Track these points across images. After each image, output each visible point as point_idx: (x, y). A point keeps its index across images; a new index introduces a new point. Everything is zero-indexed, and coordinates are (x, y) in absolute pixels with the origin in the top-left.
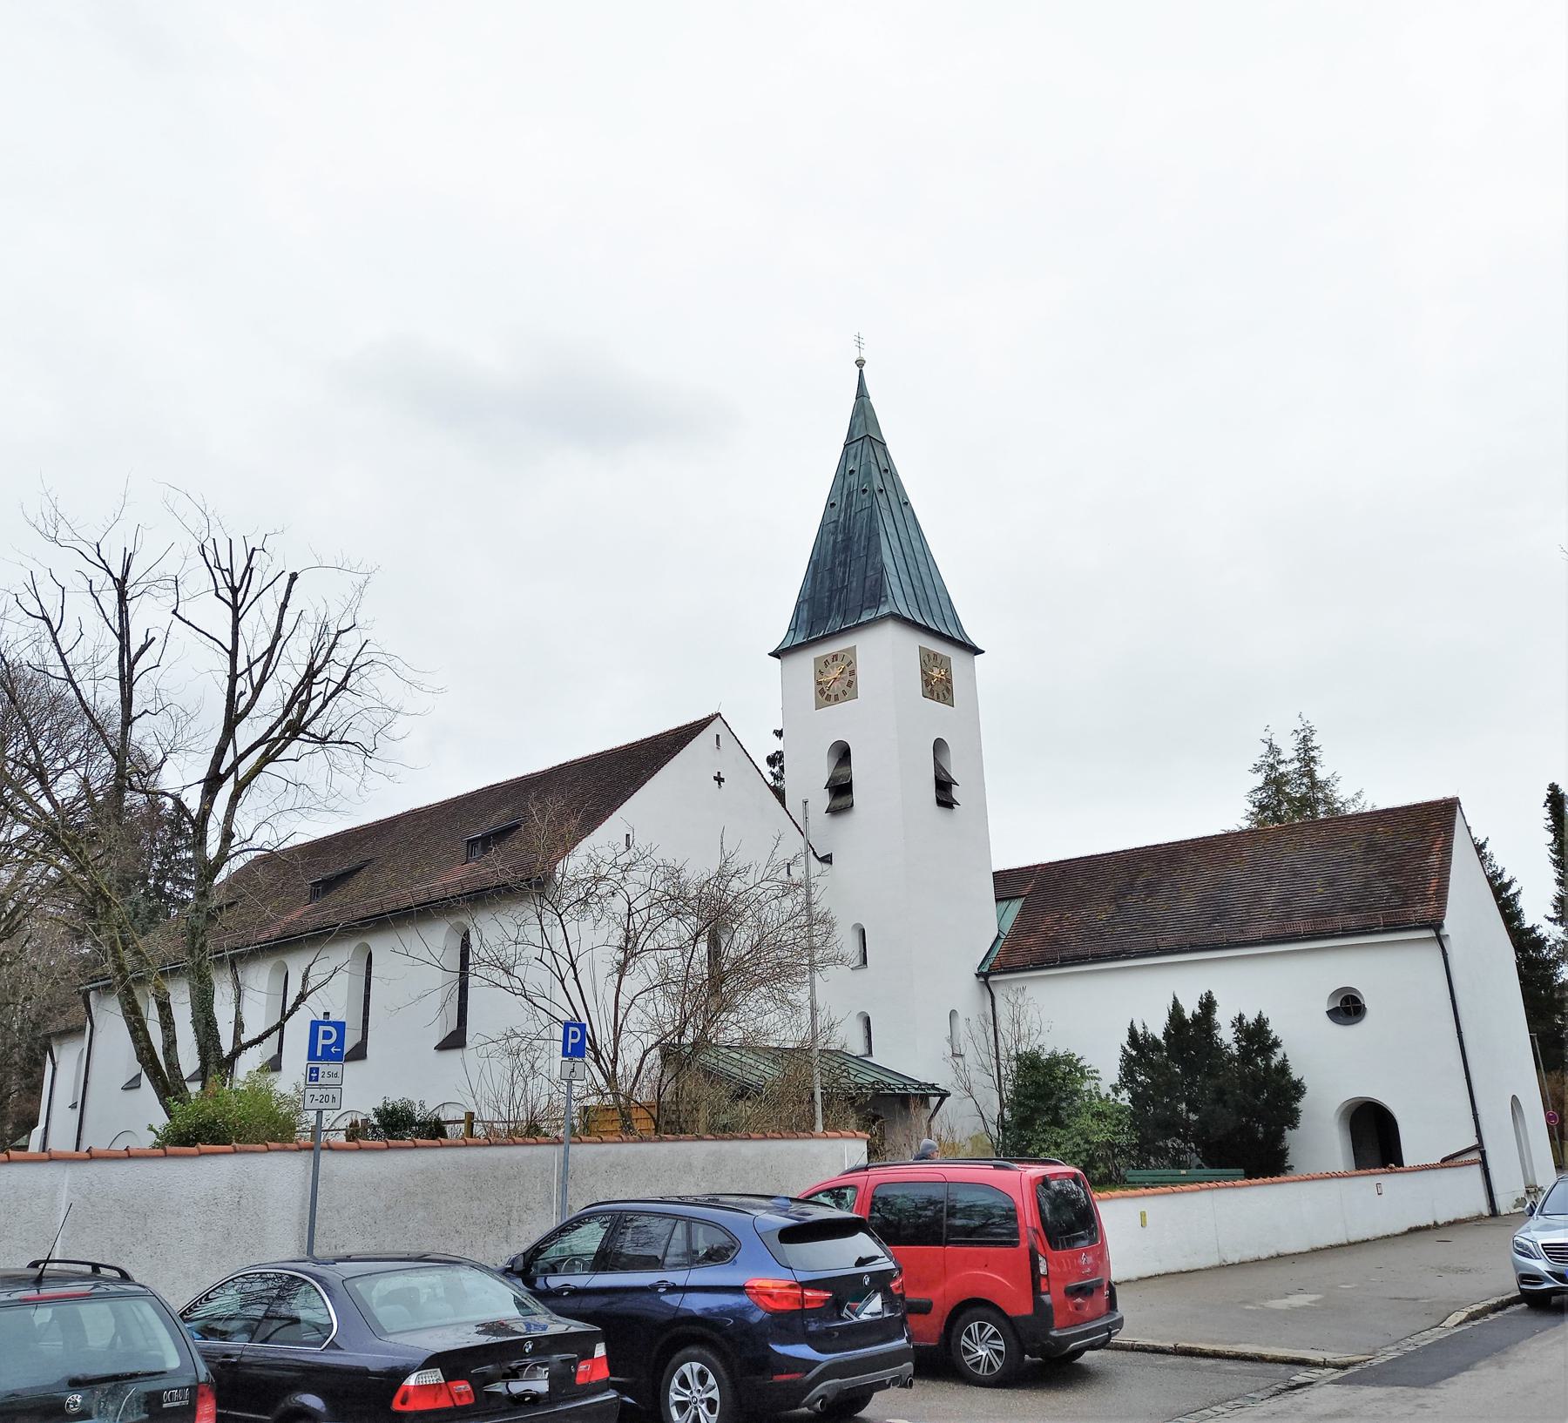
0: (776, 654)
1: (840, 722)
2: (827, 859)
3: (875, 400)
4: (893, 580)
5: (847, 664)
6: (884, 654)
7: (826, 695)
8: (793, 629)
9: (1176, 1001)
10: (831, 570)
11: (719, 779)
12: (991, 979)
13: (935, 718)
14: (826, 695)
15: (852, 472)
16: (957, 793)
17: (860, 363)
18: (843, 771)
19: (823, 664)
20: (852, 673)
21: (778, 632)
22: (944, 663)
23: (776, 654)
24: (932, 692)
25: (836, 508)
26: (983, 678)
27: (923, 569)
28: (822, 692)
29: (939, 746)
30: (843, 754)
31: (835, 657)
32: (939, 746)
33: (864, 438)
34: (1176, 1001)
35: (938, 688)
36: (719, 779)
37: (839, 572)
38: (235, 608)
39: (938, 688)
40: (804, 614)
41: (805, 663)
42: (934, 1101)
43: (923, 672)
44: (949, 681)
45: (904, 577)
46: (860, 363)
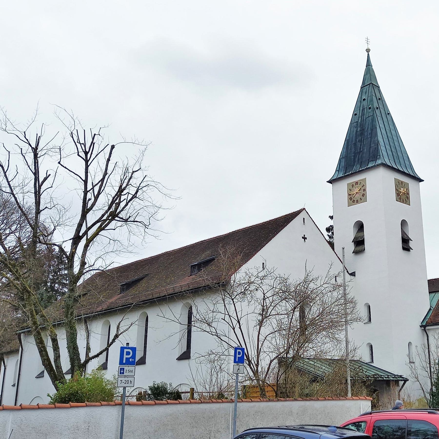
0: (330, 182)
1: (359, 212)
2: (353, 274)
3: (375, 67)
4: (383, 148)
5: (362, 186)
6: (379, 182)
7: (353, 200)
8: (338, 170)
9: (369, 83)
10: (355, 144)
11: (304, 238)
12: (427, 328)
13: (402, 211)
14: (353, 200)
15: (364, 100)
16: (411, 244)
17: (368, 51)
18: (360, 234)
19: (351, 187)
20: (364, 190)
21: (331, 172)
22: (406, 186)
23: (330, 182)
24: (400, 198)
25: (357, 116)
26: (424, 192)
27: (396, 143)
28: (351, 199)
29: (404, 223)
30: (360, 227)
31: (357, 183)
32: (404, 223)
33: (370, 84)
34: (369, 83)
35: (403, 197)
36: (304, 238)
37: (358, 144)
38: (87, 161)
39: (403, 197)
40: (343, 164)
41: (343, 185)
42: (401, 383)
43: (396, 190)
44: (408, 194)
45: (388, 147)
46: (368, 51)
